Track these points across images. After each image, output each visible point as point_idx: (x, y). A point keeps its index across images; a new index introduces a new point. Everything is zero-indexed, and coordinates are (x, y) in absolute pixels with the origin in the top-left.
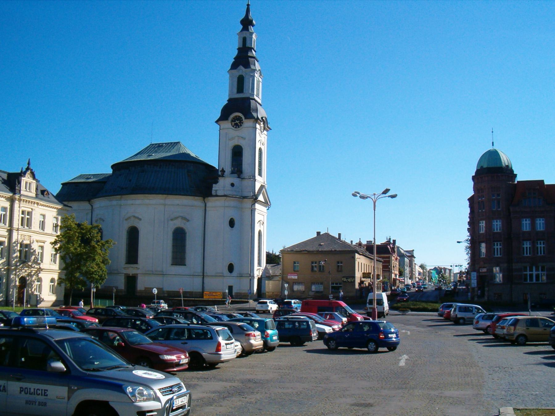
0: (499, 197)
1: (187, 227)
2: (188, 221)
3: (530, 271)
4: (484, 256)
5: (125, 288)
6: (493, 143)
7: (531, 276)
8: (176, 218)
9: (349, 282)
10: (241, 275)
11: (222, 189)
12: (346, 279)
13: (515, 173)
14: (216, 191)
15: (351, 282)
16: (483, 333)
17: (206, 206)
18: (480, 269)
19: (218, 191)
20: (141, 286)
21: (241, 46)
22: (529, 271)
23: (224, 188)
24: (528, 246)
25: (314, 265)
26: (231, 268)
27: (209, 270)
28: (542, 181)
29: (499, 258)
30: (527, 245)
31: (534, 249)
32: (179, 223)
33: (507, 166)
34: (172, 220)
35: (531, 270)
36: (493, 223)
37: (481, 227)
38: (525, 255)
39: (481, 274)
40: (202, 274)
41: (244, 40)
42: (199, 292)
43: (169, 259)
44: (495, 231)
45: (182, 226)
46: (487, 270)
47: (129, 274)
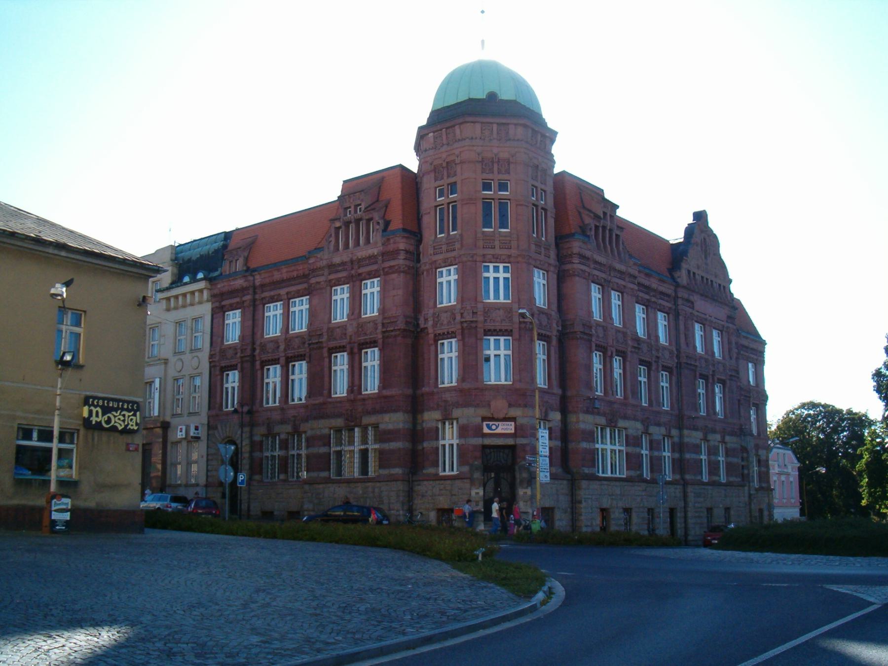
6: (483, 42)
9: (114, 429)
39: (488, 441)
44: (492, 300)
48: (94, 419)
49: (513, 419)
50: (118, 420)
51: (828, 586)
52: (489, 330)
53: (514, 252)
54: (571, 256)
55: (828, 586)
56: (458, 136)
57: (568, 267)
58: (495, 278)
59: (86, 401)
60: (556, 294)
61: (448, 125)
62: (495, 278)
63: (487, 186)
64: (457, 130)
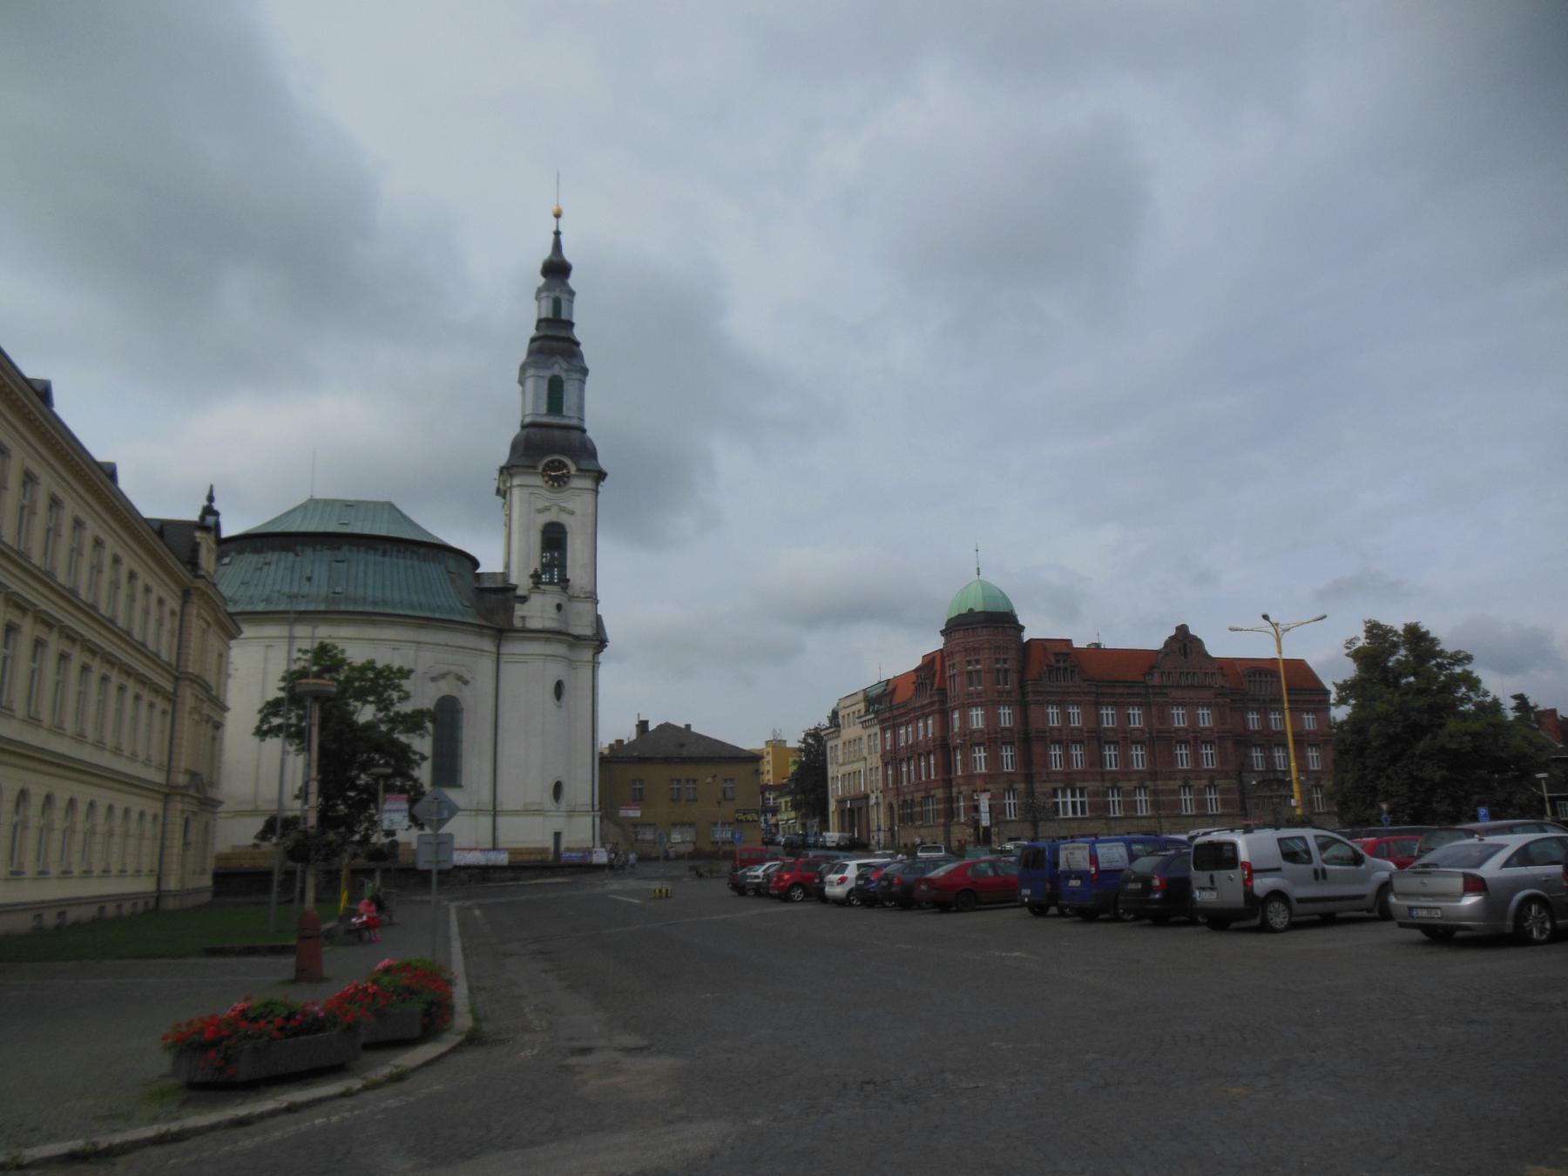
1: (466, 696)
2: (466, 683)
5: (1071, 887)
6: (978, 569)
8: (443, 676)
9: (748, 821)
11: (539, 614)
14: (523, 618)
15: (754, 821)
19: (527, 620)
22: (1062, 797)
26: (558, 789)
27: (508, 801)
28: (1068, 642)
29: (1114, 772)
34: (433, 679)
35: (1064, 795)
36: (979, 709)
40: (491, 808)
41: (557, 304)
44: (975, 727)
45: (454, 693)
49: (989, 791)
50: (749, 817)
53: (983, 700)
54: (1028, 693)
57: (1027, 699)
59: (737, 811)
63: (997, 661)
64: (980, 630)
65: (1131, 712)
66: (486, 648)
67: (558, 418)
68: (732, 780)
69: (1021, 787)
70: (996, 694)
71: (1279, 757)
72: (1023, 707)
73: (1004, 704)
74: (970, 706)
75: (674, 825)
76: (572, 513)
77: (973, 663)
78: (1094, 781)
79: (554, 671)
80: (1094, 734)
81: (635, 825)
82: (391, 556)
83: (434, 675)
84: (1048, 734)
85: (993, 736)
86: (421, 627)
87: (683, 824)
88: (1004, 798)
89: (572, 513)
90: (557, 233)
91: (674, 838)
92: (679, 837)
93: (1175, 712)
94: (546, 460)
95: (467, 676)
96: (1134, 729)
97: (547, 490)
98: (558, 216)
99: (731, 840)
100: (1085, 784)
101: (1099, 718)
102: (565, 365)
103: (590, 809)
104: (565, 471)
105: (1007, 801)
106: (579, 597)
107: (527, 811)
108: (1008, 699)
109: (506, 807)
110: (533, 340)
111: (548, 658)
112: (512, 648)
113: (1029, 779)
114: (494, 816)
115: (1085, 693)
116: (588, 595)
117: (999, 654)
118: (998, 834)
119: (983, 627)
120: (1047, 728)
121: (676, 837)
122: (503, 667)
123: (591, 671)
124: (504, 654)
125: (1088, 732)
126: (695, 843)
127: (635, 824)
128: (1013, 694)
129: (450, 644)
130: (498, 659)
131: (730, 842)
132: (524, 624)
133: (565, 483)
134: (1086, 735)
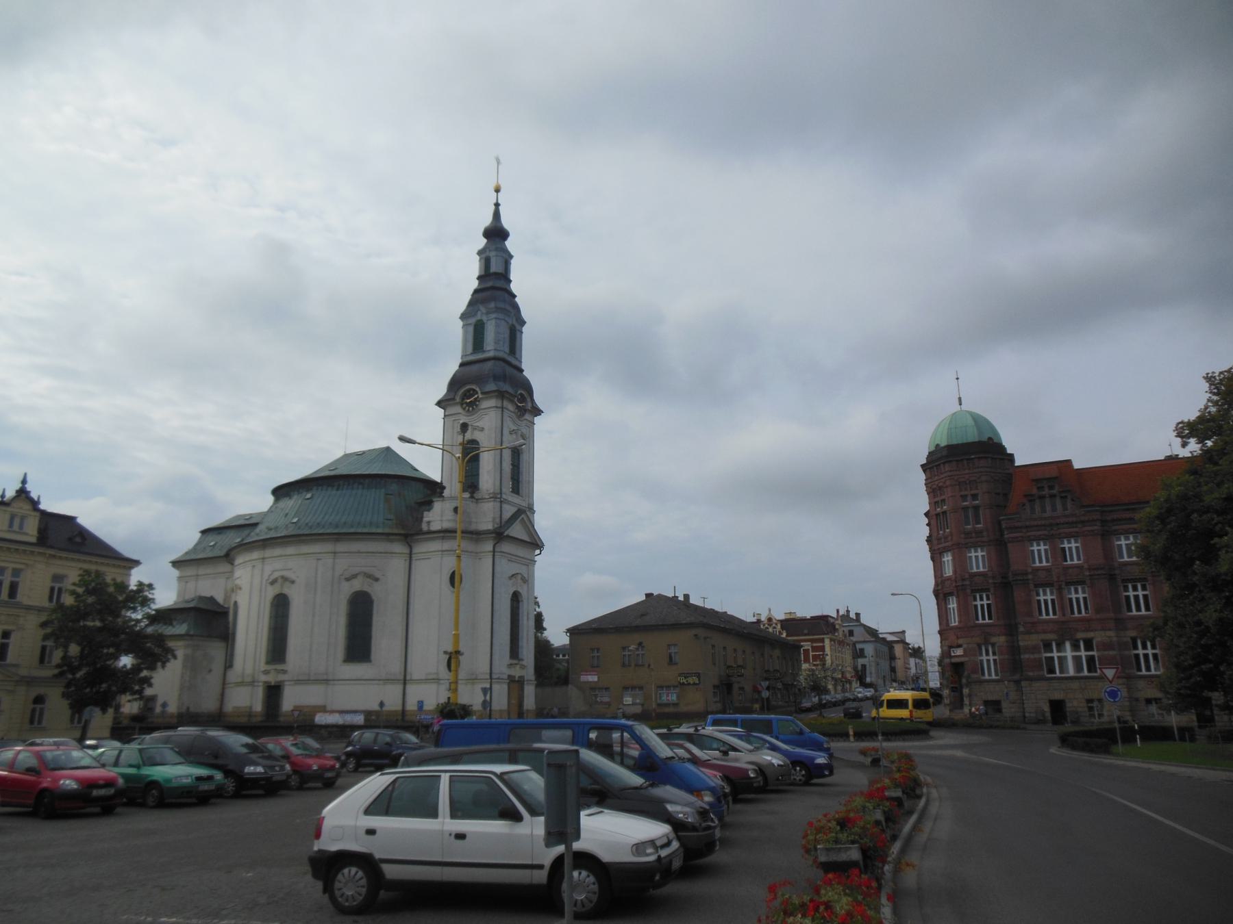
0: (965, 503)
1: (376, 591)
2: (377, 580)
3: (1059, 650)
4: (957, 624)
6: (960, 399)
7: (1062, 660)
8: (354, 576)
9: (689, 684)
10: (474, 677)
12: (685, 678)
13: (1009, 452)
14: (429, 523)
16: (196, 801)
17: (411, 551)
18: (952, 650)
20: (291, 700)
21: (483, 273)
23: (442, 516)
24: (1049, 597)
25: (673, 650)
27: (416, 672)
30: (1045, 594)
31: (1063, 604)
32: (357, 585)
33: (990, 439)
34: (348, 579)
37: (946, 562)
38: (1044, 616)
39: (954, 660)
40: (402, 678)
42: (396, 711)
43: (340, 651)
44: (975, 570)
45: (366, 588)
46: (965, 651)
47: (271, 683)
48: (681, 681)
50: (691, 680)
51: (765, 757)
52: (1069, 582)
55: (765, 757)
56: (943, 471)
58: (976, 556)
59: (680, 675)
60: (175, 633)
61: (937, 463)
62: (976, 556)
63: (964, 498)
65: (1066, 545)
66: (397, 551)
67: (480, 354)
68: (675, 645)
69: (1001, 640)
70: (963, 536)
71: (953, 604)
72: (999, 545)
73: (975, 546)
74: (968, 547)
75: (626, 688)
76: (482, 429)
77: (969, 498)
78: (1103, 629)
79: (450, 563)
80: (1103, 572)
81: (593, 689)
82: (342, 490)
83: (347, 577)
84: (1030, 577)
85: (959, 583)
86: (337, 540)
87: (633, 688)
88: (1136, 648)
89: (482, 429)
90: (497, 205)
91: (626, 701)
92: (631, 699)
93: (1035, 548)
94: (462, 390)
95: (377, 575)
96: (1038, 569)
97: (464, 415)
98: (497, 190)
99: (676, 702)
100: (1090, 635)
101: (1109, 553)
102: (483, 310)
103: (488, 677)
104: (476, 396)
105: (984, 658)
106: (485, 499)
107: (426, 681)
108: (978, 539)
109: (415, 677)
110: (476, 291)
111: (445, 553)
112: (421, 548)
113: (1011, 630)
114: (405, 684)
115: (1082, 522)
116: (491, 496)
117: (966, 490)
118: (970, 696)
119: (944, 463)
120: (1030, 570)
121: (628, 700)
122: (415, 564)
123: (491, 560)
124: (415, 554)
125: (1089, 569)
126: (643, 705)
127: (593, 688)
128: (985, 534)
129: (361, 551)
130: (411, 557)
131: (674, 704)
132: (429, 527)
133: (477, 406)
134: (991, 581)
